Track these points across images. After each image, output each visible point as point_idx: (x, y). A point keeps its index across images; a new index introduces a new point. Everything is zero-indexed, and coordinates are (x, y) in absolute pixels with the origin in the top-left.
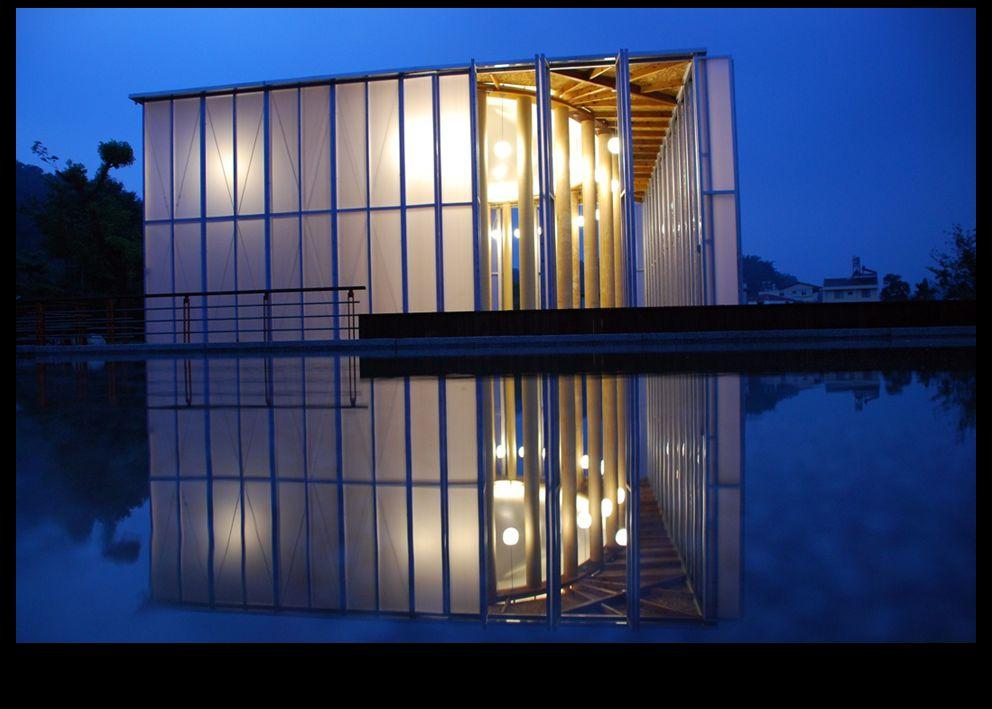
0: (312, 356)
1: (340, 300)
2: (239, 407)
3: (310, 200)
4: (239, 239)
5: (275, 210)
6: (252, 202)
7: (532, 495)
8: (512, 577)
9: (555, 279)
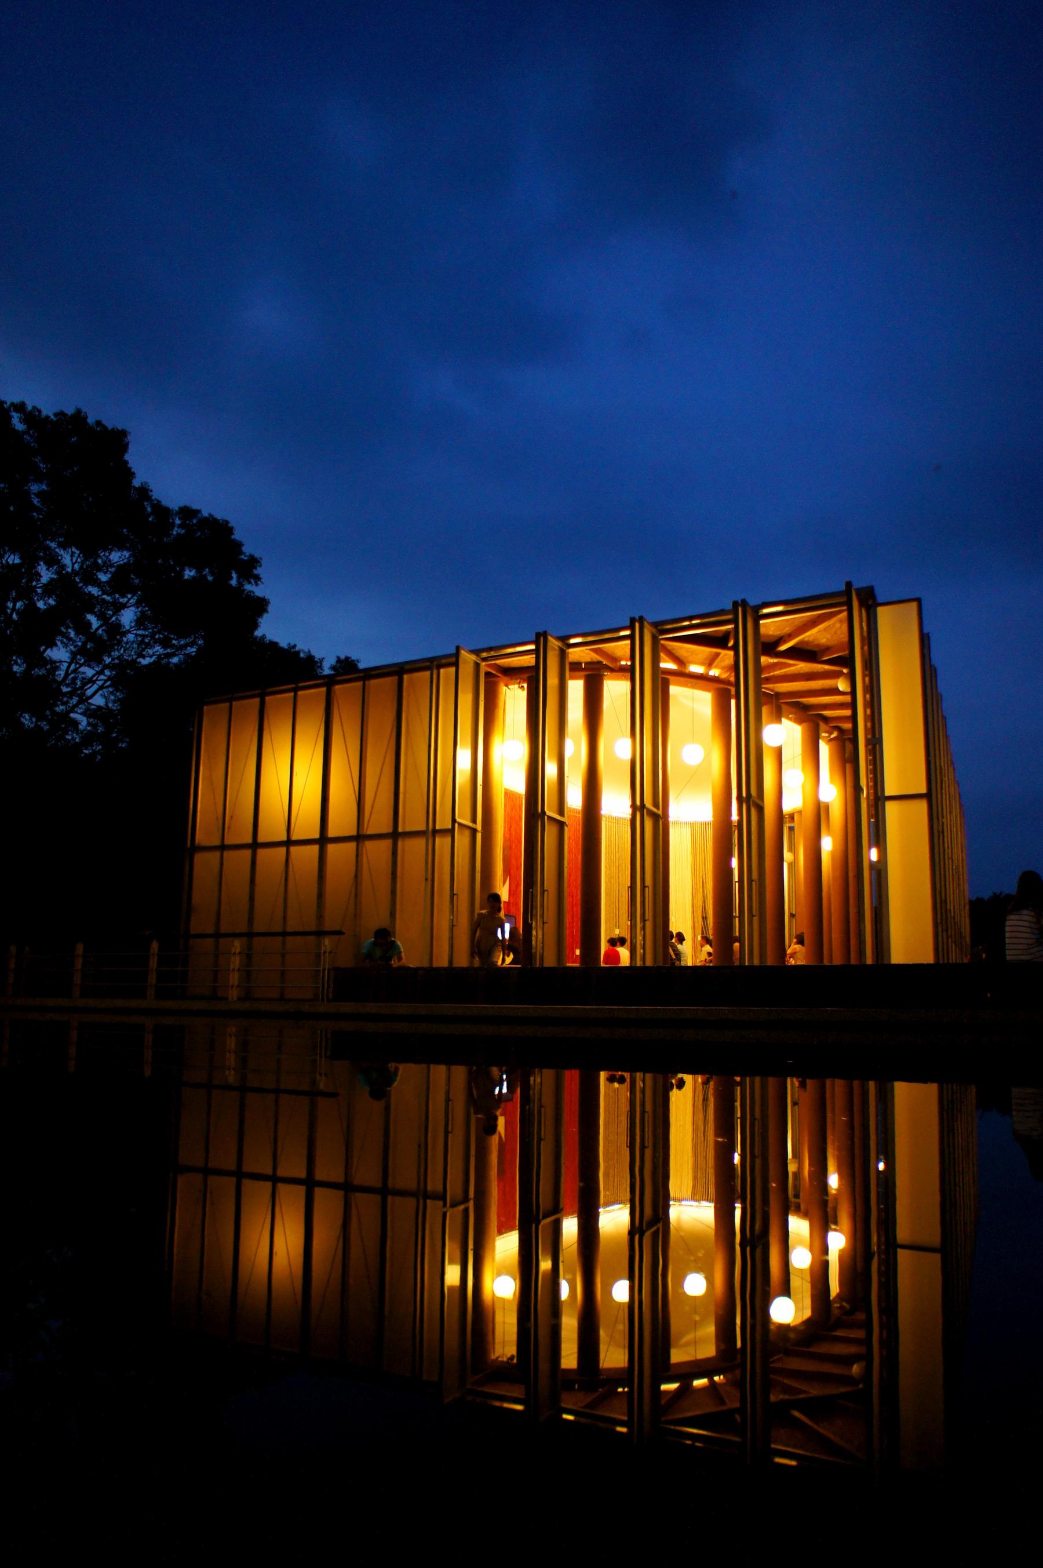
0: (866, 954)
1: (888, 793)
2: (277, 1091)
3: (368, 824)
4: (291, 873)
5: (332, 833)
6: (307, 824)
7: (724, 1215)
8: (695, 1342)
9: (765, 888)
